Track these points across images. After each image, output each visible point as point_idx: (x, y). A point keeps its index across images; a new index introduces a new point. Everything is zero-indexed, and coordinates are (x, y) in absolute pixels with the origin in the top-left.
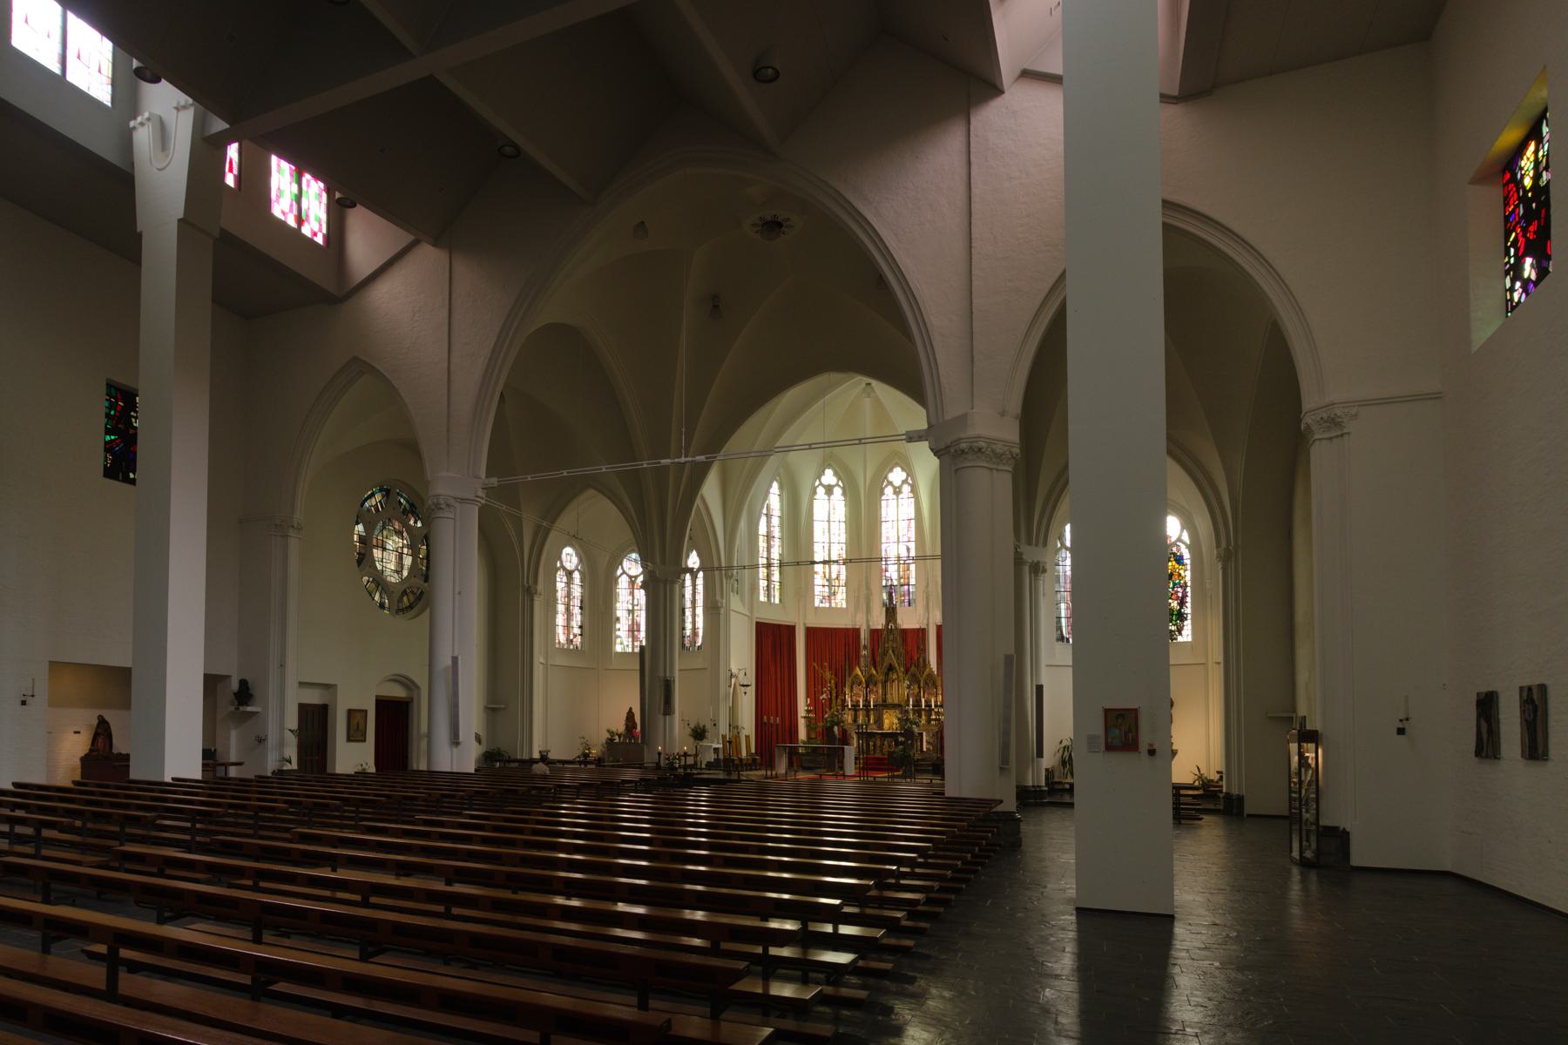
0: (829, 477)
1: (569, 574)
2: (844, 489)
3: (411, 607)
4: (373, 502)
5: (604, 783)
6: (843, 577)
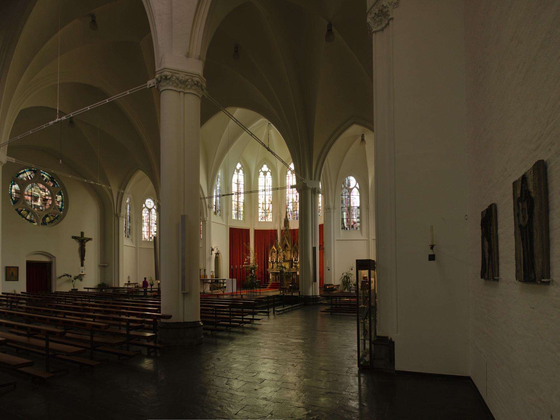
0: (265, 168)
1: (150, 210)
2: (271, 173)
3: (51, 222)
4: (25, 175)
5: (252, 288)
6: (271, 209)
